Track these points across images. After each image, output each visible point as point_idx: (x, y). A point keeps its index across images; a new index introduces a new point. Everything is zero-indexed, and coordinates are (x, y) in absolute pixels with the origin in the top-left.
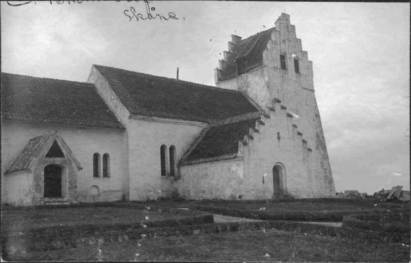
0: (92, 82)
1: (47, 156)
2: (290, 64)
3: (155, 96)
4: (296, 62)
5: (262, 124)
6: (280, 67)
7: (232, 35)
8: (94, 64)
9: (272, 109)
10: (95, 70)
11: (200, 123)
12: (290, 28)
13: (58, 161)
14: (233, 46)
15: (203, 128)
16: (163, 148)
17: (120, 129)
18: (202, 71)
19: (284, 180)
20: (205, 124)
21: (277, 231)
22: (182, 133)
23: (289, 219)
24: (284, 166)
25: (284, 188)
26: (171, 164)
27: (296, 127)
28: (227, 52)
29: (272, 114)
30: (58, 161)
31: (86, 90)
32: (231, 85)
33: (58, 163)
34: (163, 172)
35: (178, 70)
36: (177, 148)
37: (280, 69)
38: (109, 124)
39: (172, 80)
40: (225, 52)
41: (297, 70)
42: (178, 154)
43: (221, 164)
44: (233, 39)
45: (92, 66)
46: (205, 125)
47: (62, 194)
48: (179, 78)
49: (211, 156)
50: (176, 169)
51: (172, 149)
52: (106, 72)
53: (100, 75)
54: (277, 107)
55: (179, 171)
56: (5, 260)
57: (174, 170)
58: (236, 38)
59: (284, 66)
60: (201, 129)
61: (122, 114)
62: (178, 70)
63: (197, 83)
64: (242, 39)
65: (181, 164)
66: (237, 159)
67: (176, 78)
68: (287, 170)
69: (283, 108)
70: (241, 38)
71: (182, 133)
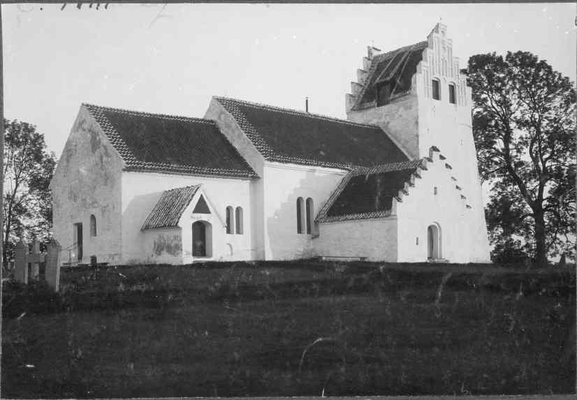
0: (214, 118)
1: (194, 212)
3: (290, 135)
5: (418, 176)
8: (221, 95)
9: (430, 160)
10: (217, 103)
13: (203, 217)
14: (370, 62)
15: (342, 177)
18: (330, 100)
22: (323, 181)
23: (154, 169)
26: (307, 218)
29: (428, 165)
30: (203, 217)
32: (371, 117)
35: (307, 101)
38: (228, 162)
41: (453, 100)
43: (369, 222)
47: (207, 252)
51: (309, 201)
54: (436, 155)
56: (317, 343)
59: (437, 96)
60: (339, 179)
62: (307, 101)
66: (389, 218)
69: (442, 158)
71: (323, 181)
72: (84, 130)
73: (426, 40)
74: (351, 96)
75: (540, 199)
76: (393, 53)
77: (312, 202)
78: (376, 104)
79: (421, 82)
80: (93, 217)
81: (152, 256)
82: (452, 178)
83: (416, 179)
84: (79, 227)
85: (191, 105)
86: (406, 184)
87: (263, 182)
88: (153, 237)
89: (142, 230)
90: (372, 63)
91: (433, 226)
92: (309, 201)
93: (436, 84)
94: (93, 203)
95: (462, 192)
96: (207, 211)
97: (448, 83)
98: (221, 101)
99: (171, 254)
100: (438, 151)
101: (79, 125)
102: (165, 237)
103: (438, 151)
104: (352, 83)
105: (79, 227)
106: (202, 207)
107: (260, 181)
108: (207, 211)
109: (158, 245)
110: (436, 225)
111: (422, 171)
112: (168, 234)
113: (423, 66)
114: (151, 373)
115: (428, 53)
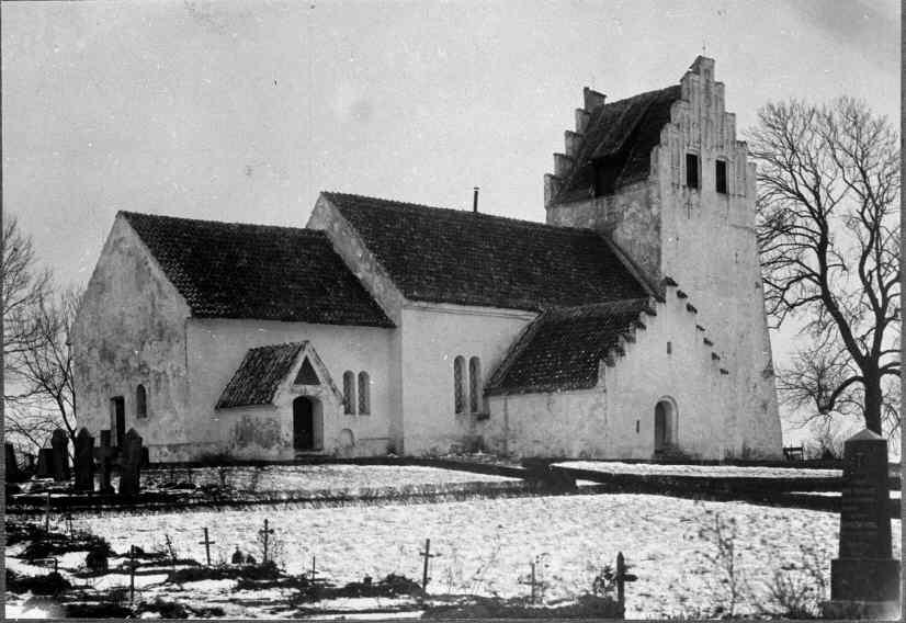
1: (295, 383)
2: (708, 175)
4: (721, 168)
6: (685, 183)
7: (586, 89)
11: (525, 313)
12: (713, 90)
13: (310, 390)
14: (588, 117)
15: (526, 323)
16: (458, 361)
17: (379, 320)
18: (519, 193)
19: (674, 428)
20: (531, 313)
21: (261, 449)
22: (489, 332)
24: (676, 404)
25: (674, 440)
27: (702, 329)
28: (575, 134)
30: (310, 390)
31: (311, 242)
33: (312, 393)
34: (459, 408)
35: (476, 193)
36: (481, 361)
37: (684, 187)
38: (366, 314)
39: (465, 215)
40: (569, 134)
41: (722, 187)
42: (485, 371)
44: (587, 101)
45: (318, 195)
46: (533, 317)
48: (480, 210)
49: (525, 354)
50: (480, 401)
51: (474, 362)
52: (350, 207)
53: (338, 214)
55: (486, 405)
57: (476, 405)
58: (592, 96)
59: (693, 180)
61: (380, 285)
62: (476, 193)
63: (512, 217)
64: (607, 101)
65: (488, 392)
67: (472, 210)
68: (680, 411)
69: (681, 295)
70: (604, 96)
71: (489, 332)
72: (121, 252)
73: (679, 84)
74: (552, 177)
75: (877, 352)
76: (626, 102)
77: (479, 364)
78: (593, 194)
79: (667, 162)
80: (141, 389)
81: (233, 446)
82: (698, 327)
83: (637, 330)
84: (119, 402)
85: (284, 204)
86: (621, 338)
87: (400, 333)
88: (234, 418)
89: (216, 408)
90: (591, 119)
91: (667, 403)
92: (474, 362)
93: (693, 162)
94: (140, 367)
95: (713, 349)
96: (314, 380)
97: (715, 155)
98: (327, 196)
99: (137, 548)
100: (676, 285)
101: (112, 246)
102: (253, 421)
103: (676, 285)
104: (555, 155)
105: (119, 402)
106: (308, 375)
107: (398, 329)
108: (314, 380)
109: (242, 431)
110: (670, 400)
111: (647, 316)
112: (259, 415)
113: (669, 134)
114: (196, 501)
115: (679, 112)
